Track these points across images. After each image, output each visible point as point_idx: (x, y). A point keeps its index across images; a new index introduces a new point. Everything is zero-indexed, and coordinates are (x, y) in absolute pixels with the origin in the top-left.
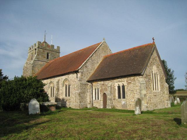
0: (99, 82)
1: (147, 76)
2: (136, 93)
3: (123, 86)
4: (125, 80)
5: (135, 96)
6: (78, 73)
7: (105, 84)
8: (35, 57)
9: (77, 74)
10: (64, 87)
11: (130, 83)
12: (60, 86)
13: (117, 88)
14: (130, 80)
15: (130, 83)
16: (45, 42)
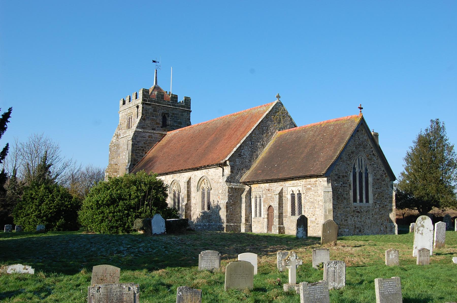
0: (263, 185)
1: (339, 178)
2: (317, 206)
3: (299, 195)
4: (302, 182)
5: (317, 213)
6: (224, 167)
7: (271, 190)
8: (136, 125)
9: (223, 169)
10: (200, 193)
11: (310, 189)
12: (193, 189)
13: (289, 197)
14: (309, 184)
15: (310, 189)
16: (156, 88)
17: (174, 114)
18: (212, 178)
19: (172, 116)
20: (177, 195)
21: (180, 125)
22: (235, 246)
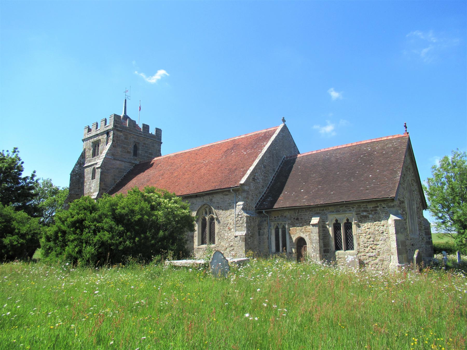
17: (145, 144)
18: (218, 206)
19: (143, 146)
20: (412, 196)
21: (150, 156)
22: (407, 313)
